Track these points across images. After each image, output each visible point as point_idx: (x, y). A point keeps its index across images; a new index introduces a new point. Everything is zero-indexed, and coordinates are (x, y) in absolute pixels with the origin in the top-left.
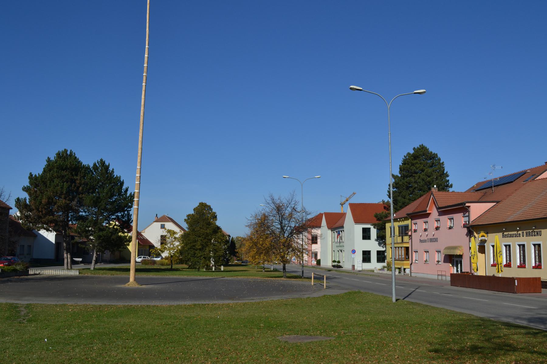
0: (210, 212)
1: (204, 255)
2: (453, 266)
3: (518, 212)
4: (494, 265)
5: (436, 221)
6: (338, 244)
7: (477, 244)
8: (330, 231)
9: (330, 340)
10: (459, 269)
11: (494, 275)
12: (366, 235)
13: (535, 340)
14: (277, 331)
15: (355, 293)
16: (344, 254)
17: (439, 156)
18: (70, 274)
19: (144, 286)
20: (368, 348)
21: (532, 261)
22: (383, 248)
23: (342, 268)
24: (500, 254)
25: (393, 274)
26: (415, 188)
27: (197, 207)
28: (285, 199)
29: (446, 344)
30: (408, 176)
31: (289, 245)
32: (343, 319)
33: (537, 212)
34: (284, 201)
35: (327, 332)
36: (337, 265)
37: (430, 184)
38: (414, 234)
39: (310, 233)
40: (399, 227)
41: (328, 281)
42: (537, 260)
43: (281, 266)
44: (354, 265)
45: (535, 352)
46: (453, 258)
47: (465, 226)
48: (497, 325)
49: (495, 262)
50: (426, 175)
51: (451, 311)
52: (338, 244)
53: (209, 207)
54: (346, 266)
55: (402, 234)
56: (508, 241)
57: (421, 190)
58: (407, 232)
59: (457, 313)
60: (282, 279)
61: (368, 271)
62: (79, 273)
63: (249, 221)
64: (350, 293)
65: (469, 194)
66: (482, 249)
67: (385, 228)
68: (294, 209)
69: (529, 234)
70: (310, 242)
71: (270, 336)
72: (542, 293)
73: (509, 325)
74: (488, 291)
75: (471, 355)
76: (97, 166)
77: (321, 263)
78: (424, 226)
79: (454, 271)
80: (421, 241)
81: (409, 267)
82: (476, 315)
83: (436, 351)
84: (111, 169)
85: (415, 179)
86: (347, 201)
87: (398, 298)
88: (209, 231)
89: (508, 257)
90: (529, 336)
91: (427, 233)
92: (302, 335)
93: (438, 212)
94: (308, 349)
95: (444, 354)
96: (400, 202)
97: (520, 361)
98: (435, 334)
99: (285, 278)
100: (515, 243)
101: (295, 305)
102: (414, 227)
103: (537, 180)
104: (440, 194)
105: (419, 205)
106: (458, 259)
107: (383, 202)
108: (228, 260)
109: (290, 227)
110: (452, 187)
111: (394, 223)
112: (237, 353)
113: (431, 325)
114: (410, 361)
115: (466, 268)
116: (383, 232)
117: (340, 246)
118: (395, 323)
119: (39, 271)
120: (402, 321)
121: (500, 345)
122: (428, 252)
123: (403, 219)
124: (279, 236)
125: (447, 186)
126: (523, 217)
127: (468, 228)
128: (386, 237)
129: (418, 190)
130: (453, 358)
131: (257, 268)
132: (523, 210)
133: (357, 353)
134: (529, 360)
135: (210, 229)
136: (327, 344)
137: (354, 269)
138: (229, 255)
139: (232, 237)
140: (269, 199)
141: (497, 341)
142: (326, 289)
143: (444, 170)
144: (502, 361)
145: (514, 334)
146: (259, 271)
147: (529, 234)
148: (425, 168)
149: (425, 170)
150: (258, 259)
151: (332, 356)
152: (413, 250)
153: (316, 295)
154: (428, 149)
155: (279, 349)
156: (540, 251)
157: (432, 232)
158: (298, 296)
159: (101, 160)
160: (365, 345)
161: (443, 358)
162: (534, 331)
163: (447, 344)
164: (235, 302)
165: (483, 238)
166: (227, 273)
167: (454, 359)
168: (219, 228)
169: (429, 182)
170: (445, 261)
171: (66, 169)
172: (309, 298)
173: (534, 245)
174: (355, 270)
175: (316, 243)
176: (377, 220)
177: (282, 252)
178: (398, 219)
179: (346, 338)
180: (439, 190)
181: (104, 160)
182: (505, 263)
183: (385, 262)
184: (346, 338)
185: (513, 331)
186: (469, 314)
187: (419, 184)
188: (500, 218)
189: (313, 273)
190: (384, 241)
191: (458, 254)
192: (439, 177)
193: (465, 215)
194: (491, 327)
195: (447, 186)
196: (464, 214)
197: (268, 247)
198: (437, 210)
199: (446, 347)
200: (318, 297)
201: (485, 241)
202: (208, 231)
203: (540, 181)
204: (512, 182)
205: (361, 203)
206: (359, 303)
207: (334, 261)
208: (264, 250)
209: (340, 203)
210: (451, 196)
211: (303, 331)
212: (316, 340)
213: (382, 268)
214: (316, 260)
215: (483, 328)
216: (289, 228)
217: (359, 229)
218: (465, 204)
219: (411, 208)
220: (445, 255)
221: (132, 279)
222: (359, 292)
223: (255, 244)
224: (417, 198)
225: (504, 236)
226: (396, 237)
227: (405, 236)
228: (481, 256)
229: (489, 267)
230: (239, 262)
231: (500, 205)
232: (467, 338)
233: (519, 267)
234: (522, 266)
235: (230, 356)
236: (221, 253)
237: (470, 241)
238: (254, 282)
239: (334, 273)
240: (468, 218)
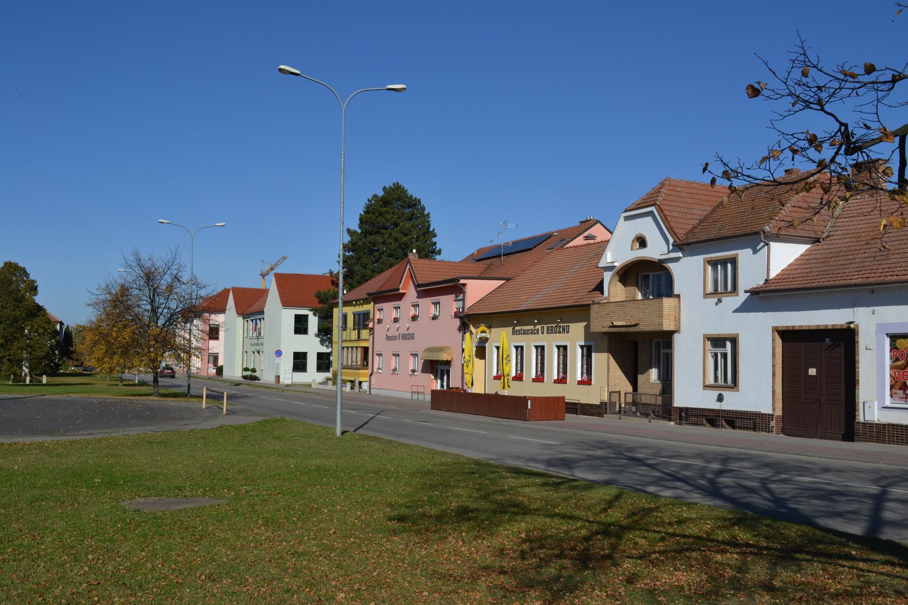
0: (25, 279)
1: (9, 355)
2: (436, 378)
3: (537, 296)
4: (497, 378)
5: (413, 306)
6: (255, 341)
7: (474, 344)
8: (241, 319)
9: (219, 505)
10: (445, 384)
11: (497, 392)
12: (301, 326)
13: (555, 494)
14: (124, 490)
15: (276, 421)
16: (262, 357)
17: (422, 203)
20: (285, 518)
21: (553, 372)
22: (328, 348)
23: (259, 380)
24: (507, 360)
25: (339, 390)
26: (383, 253)
28: (160, 260)
29: (417, 507)
30: (373, 232)
31: (165, 339)
32: (247, 466)
33: (565, 296)
34: (160, 264)
35: (215, 489)
36: (251, 375)
37: (407, 247)
38: (377, 327)
39: (206, 321)
40: (354, 315)
41: (231, 402)
42: (561, 370)
43: (149, 378)
44: (279, 376)
45: (557, 515)
46: (436, 366)
47: (456, 315)
48: (499, 472)
49: (500, 373)
50: (401, 232)
51: (430, 449)
52: (255, 341)
53: (24, 270)
54: (267, 377)
55: (359, 326)
56: (521, 340)
57: (392, 257)
58: (367, 323)
59: (437, 453)
60: (152, 398)
61: (302, 385)
63: (93, 297)
64: (267, 421)
65: (466, 265)
66: (481, 352)
67: (331, 316)
68: (176, 278)
69: (552, 330)
70: (207, 337)
71: (108, 500)
72: (566, 420)
73: (517, 472)
74: (486, 417)
75: (456, 524)
77: (225, 373)
78: (394, 314)
79: (437, 386)
80: (389, 338)
81: (367, 379)
82: (467, 456)
83: (401, 519)
85: (383, 237)
86: (272, 269)
87: (346, 429)
88: (19, 313)
89: (519, 364)
90: (548, 488)
91: (398, 326)
92: (169, 497)
93: (417, 292)
94: (175, 522)
95: (412, 523)
96: (358, 275)
97: (533, 530)
98: (400, 489)
99: (157, 397)
100: (530, 343)
101: (166, 443)
102: (378, 315)
103: (567, 248)
104: (421, 262)
105: (388, 280)
106: (445, 368)
107: (331, 273)
108: (58, 366)
109: (169, 308)
110: (440, 254)
111: (344, 308)
112: (34, 536)
113: (395, 474)
114: (354, 538)
115: (455, 383)
116: (328, 322)
117: (257, 345)
118: (336, 471)
120: (349, 468)
121: (503, 505)
122: (398, 355)
123: (362, 301)
124: (147, 323)
125: (433, 252)
126: (544, 304)
127: (461, 318)
128: (332, 331)
129: (387, 256)
130: (427, 530)
132: (545, 293)
133: (263, 528)
134: (548, 529)
135: (21, 309)
136: (212, 512)
137: (279, 382)
138: (59, 356)
139: (68, 326)
140: (132, 258)
141: (499, 497)
142: (227, 414)
143: (429, 226)
144: (506, 532)
145: (525, 486)
146: (112, 385)
147: (552, 330)
148: (400, 221)
149: (399, 225)
150: (108, 363)
151: (217, 534)
152: (375, 353)
153: (207, 425)
154: (407, 191)
155: (119, 525)
156: (567, 356)
157: (405, 324)
158: (175, 427)
160: (280, 511)
161: (411, 531)
162: (555, 480)
163: (419, 505)
164: (56, 438)
165: (484, 335)
166: (51, 387)
167: (428, 531)
168: (40, 309)
169: (405, 244)
170: (424, 371)
172: (194, 430)
173: (558, 347)
174: (281, 383)
175: (217, 338)
176: (319, 303)
177: (152, 352)
178: (353, 301)
179: (247, 501)
180: (420, 257)
182: (513, 374)
183: (329, 372)
184: (247, 501)
185: (523, 480)
186: (457, 455)
187: (389, 246)
188: (509, 304)
189: (205, 389)
190: (330, 337)
191: (445, 359)
192: (422, 237)
193: (458, 298)
194: (491, 476)
195: (433, 252)
196: (457, 296)
197: (127, 343)
198: (416, 289)
199: (416, 511)
200: (211, 429)
201: (486, 340)
202: (18, 313)
203: (571, 249)
204: (530, 249)
205: (295, 274)
206: (279, 438)
207: (246, 369)
208: (120, 348)
209: (260, 272)
210: (439, 267)
211: (172, 490)
212: (192, 506)
213: (325, 381)
214: (215, 366)
215: (478, 477)
216: (165, 311)
217: (289, 316)
218: (459, 281)
219: (374, 285)
220: (425, 360)
222: (283, 420)
223: (105, 336)
224: (385, 268)
225: (515, 333)
226: (348, 330)
227: (364, 329)
228: (479, 363)
229: (490, 379)
230: (79, 370)
231: (510, 283)
232: (452, 495)
233: (534, 380)
234: (539, 379)
235: (17, 542)
236: (41, 353)
237: (463, 340)
238: (99, 403)
239: (245, 389)
240: (462, 302)
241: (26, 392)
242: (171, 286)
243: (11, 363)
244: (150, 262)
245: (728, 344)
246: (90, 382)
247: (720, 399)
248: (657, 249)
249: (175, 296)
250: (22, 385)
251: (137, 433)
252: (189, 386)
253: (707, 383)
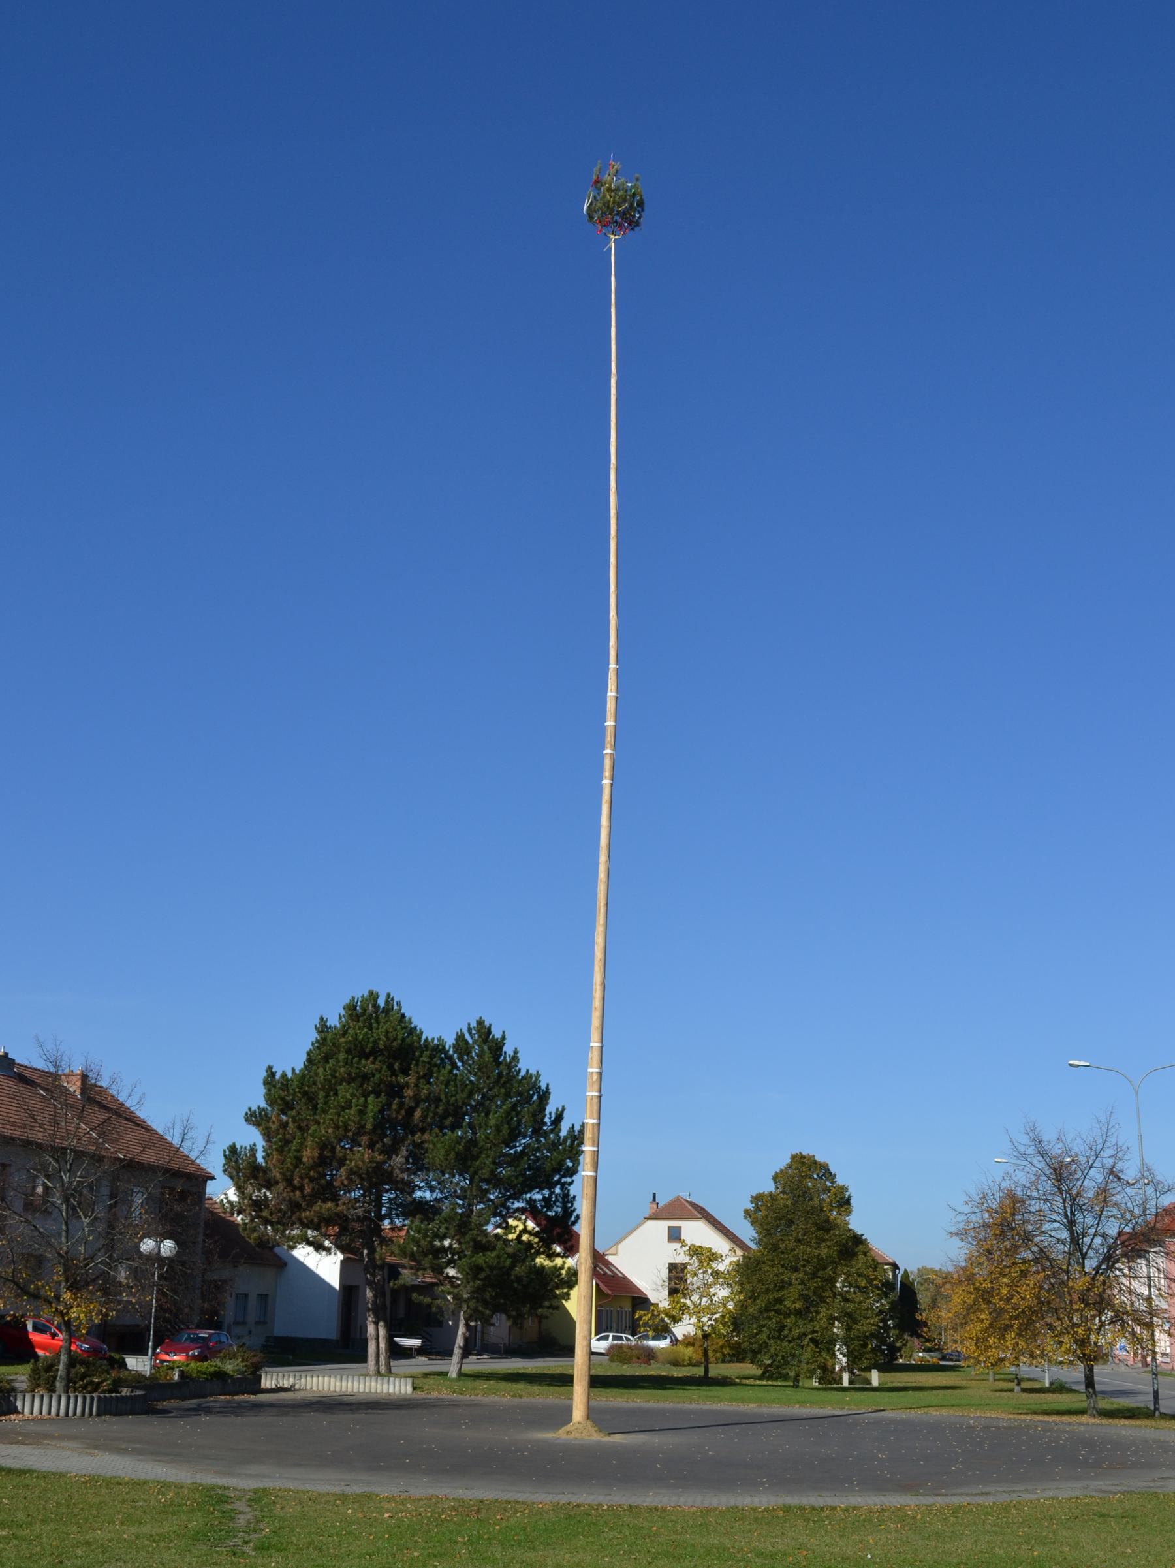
0: (829, 1184)
1: (813, 1332)
19: (618, 1438)
28: (1079, 1140)
31: (1102, 1299)
34: (1078, 1147)
60: (1085, 1419)
62: (414, 1389)
76: (467, 1042)
84: (508, 1049)
88: (826, 1251)
101: (1135, 1518)
108: (894, 1351)
109: (1104, 1236)
119: (291, 1380)
124: (1064, 1267)
140: (1026, 1140)
146: (1001, 1391)
158: (1144, 1484)
159: (480, 1023)
168: (858, 1240)
171: (374, 1053)
181: (487, 1024)
197: (1030, 1308)
202: (824, 1252)
216: (1098, 1240)
230: (932, 1358)
237: (1128, 1168)
242: (1105, 1190)
243: (817, 1346)
244: (1061, 1145)
249: (1115, 1212)
251: (1073, 1495)
252: (1156, 1395)
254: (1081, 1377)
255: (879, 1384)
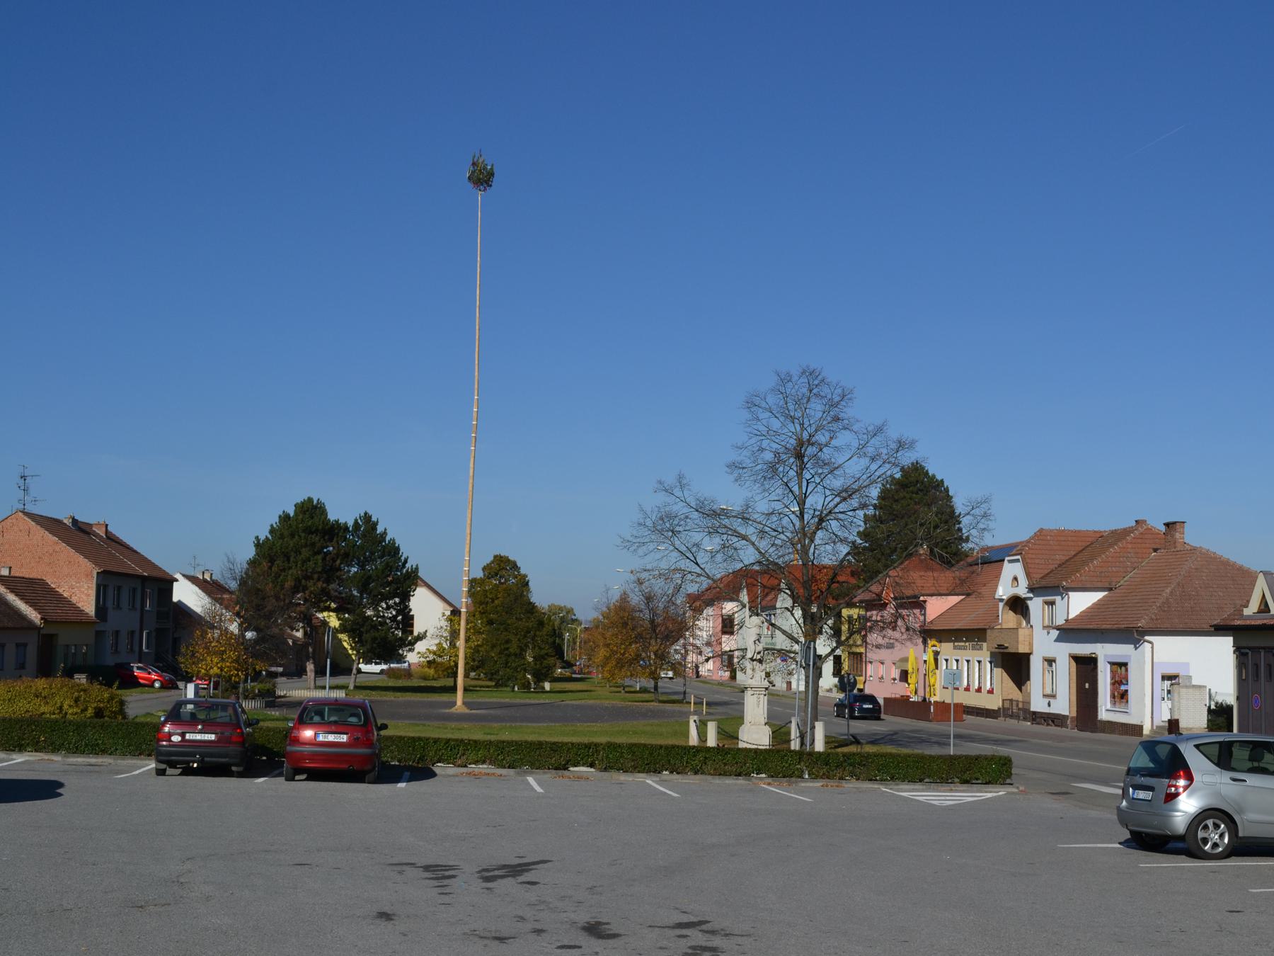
18: (335, 696)
19: (473, 711)
27: (488, 563)
41: (696, 706)
60: (652, 703)
62: (346, 695)
84: (380, 529)
119: (285, 692)
131: (610, 687)
159: (366, 513)
171: (316, 531)
181: (374, 519)
189: (692, 696)
202: (530, 625)
221: (459, 702)
225: (955, 648)
230: (567, 673)
241: (543, 699)
245: (1054, 664)
246: (589, 689)
247: (1049, 705)
248: (1022, 591)
250: (527, 692)
253: (1045, 693)
254: (653, 686)
255: (551, 689)
